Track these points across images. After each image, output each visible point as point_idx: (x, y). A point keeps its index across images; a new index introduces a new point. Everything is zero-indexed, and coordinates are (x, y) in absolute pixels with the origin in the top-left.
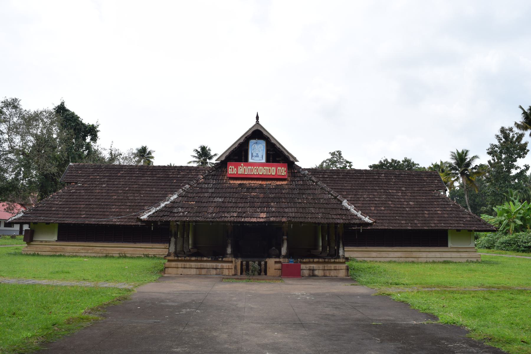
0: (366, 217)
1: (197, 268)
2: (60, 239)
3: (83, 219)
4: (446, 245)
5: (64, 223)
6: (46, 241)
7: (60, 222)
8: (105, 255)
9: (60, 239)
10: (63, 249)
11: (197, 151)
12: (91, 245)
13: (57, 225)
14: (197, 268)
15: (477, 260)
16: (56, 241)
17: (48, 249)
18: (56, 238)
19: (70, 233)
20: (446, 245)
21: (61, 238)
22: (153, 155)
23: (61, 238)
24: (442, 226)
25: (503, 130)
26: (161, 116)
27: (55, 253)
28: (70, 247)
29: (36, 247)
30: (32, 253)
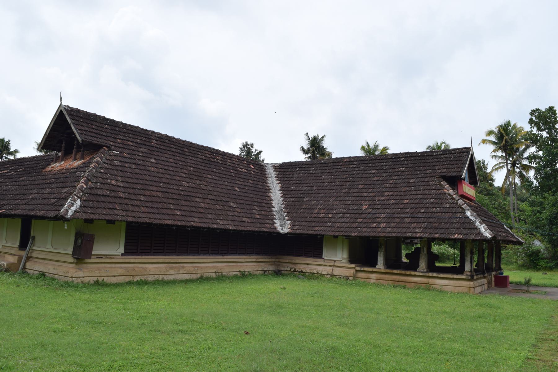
0: (481, 224)
1: (480, 286)
2: (128, 251)
3: (174, 216)
4: (320, 256)
6: (106, 256)
9: (128, 251)
10: (145, 269)
11: (377, 146)
13: (124, 225)
14: (480, 286)
15: (97, 281)
16: (122, 255)
17: (121, 271)
18: (122, 250)
19: (145, 239)
20: (320, 256)
22: (372, 146)
24: (317, 230)
25: (246, 143)
26: (256, 98)
27: (131, 279)
28: (154, 266)
29: (99, 269)
30: (92, 280)
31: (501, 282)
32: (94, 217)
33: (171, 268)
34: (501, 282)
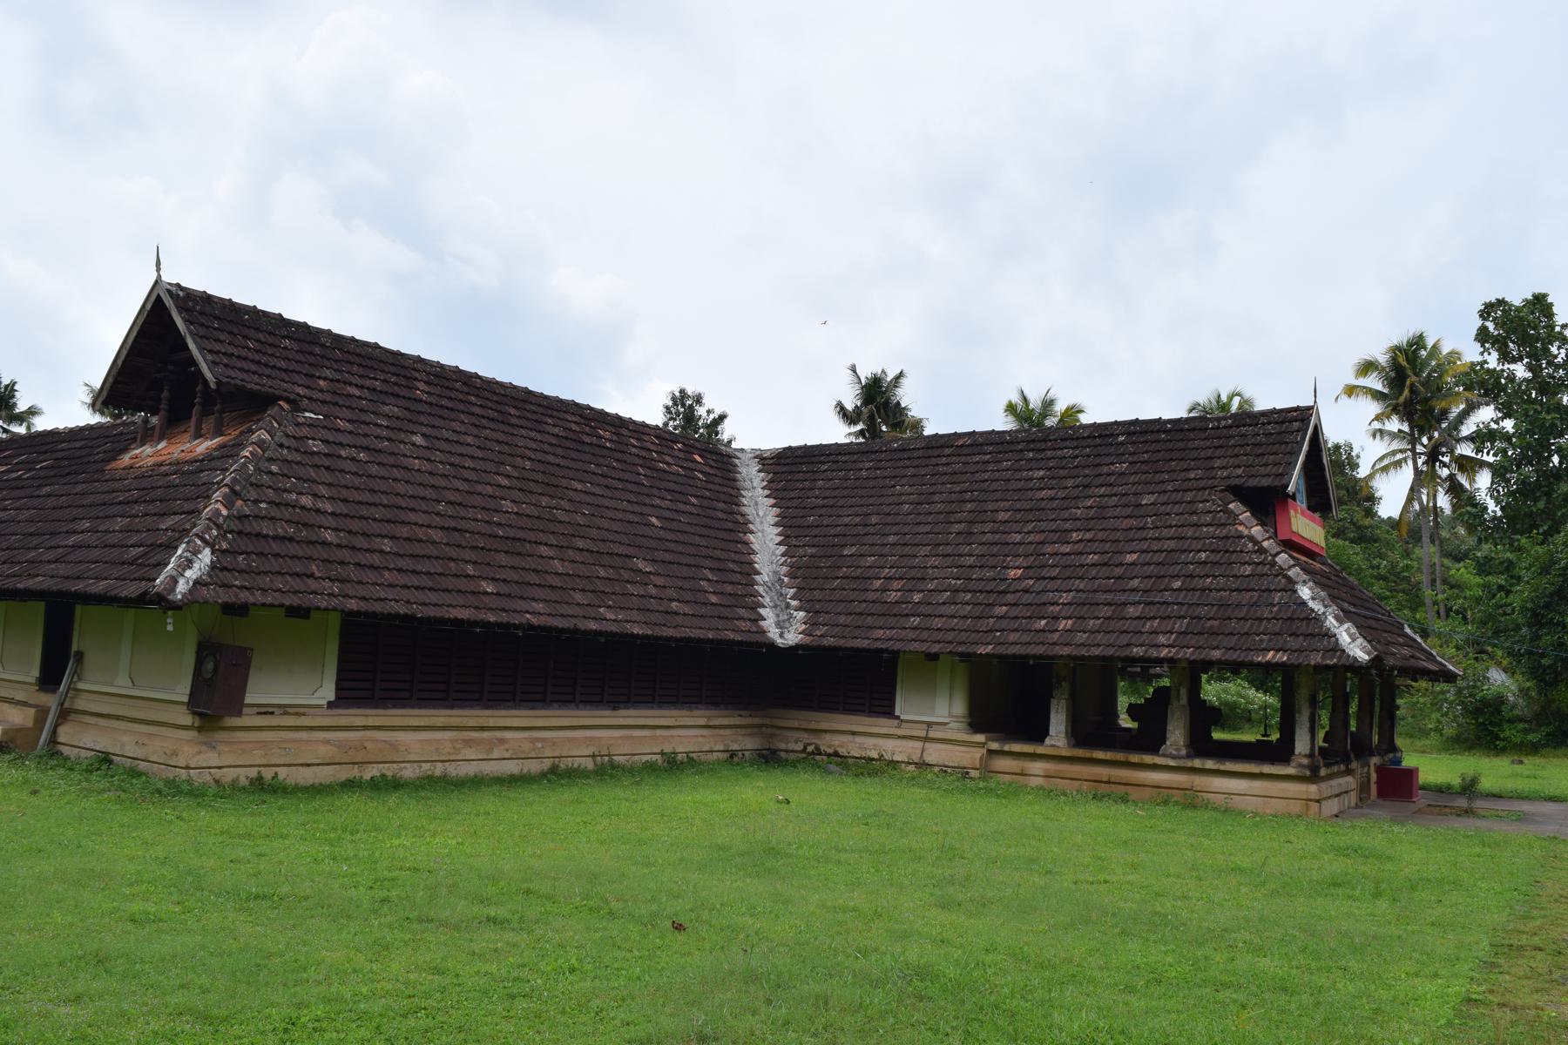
0: (1341, 622)
2: (347, 696)
3: (478, 597)
4: (887, 710)
5: (442, 621)
6: (285, 709)
7: (353, 605)
8: (547, 764)
9: (347, 696)
10: (394, 746)
11: (1052, 402)
12: (492, 722)
13: (334, 622)
16: (331, 705)
17: (325, 752)
18: (328, 692)
19: (396, 662)
20: (887, 710)
21: (358, 688)
22: (1035, 402)
23: (358, 688)
24: (880, 637)
25: (682, 391)
26: (712, 270)
27: (354, 772)
28: (419, 737)
29: (264, 744)
30: (244, 775)
31: (1397, 786)
32: (251, 600)
33: (468, 743)
34: (1397, 786)
